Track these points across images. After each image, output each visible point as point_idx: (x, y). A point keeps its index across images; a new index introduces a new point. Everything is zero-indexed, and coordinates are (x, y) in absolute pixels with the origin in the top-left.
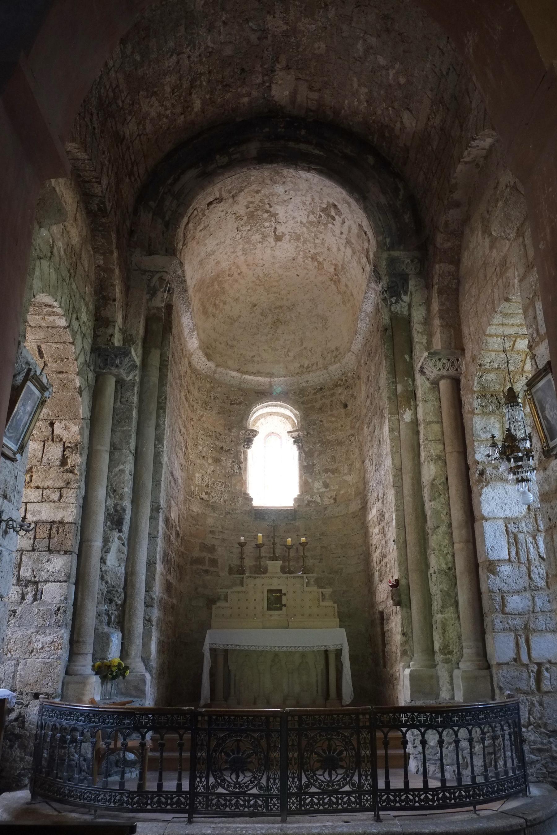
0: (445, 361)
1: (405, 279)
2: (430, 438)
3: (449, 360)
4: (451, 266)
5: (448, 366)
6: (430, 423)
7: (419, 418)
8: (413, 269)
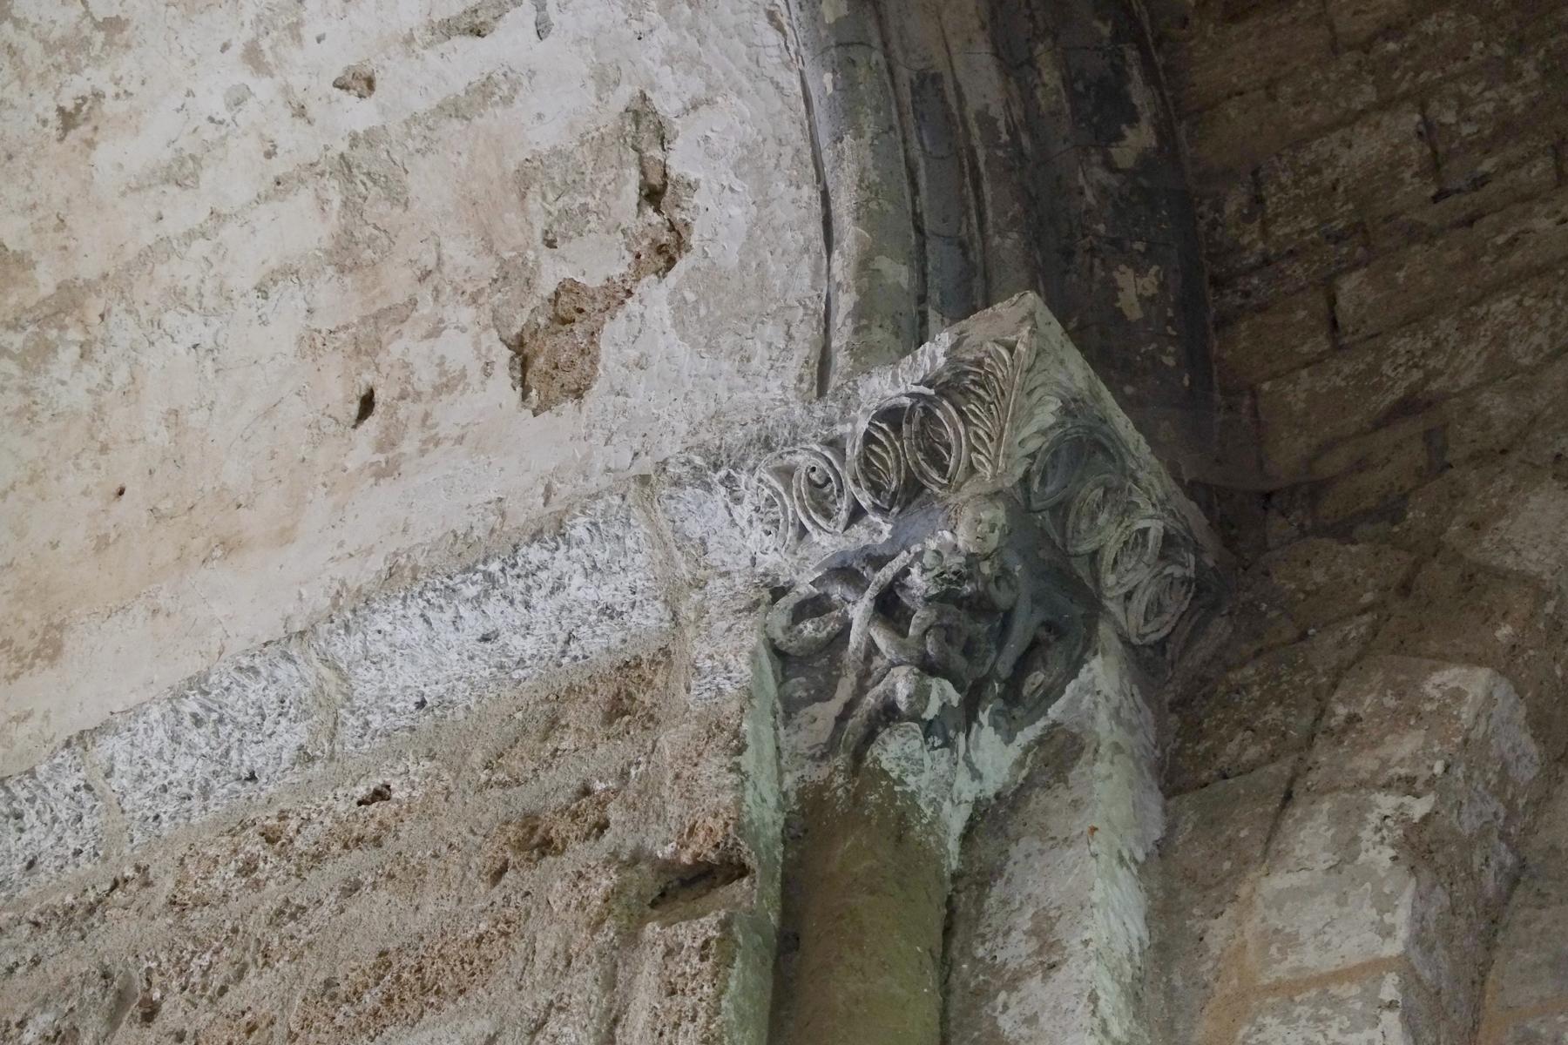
8: (1140, 604)
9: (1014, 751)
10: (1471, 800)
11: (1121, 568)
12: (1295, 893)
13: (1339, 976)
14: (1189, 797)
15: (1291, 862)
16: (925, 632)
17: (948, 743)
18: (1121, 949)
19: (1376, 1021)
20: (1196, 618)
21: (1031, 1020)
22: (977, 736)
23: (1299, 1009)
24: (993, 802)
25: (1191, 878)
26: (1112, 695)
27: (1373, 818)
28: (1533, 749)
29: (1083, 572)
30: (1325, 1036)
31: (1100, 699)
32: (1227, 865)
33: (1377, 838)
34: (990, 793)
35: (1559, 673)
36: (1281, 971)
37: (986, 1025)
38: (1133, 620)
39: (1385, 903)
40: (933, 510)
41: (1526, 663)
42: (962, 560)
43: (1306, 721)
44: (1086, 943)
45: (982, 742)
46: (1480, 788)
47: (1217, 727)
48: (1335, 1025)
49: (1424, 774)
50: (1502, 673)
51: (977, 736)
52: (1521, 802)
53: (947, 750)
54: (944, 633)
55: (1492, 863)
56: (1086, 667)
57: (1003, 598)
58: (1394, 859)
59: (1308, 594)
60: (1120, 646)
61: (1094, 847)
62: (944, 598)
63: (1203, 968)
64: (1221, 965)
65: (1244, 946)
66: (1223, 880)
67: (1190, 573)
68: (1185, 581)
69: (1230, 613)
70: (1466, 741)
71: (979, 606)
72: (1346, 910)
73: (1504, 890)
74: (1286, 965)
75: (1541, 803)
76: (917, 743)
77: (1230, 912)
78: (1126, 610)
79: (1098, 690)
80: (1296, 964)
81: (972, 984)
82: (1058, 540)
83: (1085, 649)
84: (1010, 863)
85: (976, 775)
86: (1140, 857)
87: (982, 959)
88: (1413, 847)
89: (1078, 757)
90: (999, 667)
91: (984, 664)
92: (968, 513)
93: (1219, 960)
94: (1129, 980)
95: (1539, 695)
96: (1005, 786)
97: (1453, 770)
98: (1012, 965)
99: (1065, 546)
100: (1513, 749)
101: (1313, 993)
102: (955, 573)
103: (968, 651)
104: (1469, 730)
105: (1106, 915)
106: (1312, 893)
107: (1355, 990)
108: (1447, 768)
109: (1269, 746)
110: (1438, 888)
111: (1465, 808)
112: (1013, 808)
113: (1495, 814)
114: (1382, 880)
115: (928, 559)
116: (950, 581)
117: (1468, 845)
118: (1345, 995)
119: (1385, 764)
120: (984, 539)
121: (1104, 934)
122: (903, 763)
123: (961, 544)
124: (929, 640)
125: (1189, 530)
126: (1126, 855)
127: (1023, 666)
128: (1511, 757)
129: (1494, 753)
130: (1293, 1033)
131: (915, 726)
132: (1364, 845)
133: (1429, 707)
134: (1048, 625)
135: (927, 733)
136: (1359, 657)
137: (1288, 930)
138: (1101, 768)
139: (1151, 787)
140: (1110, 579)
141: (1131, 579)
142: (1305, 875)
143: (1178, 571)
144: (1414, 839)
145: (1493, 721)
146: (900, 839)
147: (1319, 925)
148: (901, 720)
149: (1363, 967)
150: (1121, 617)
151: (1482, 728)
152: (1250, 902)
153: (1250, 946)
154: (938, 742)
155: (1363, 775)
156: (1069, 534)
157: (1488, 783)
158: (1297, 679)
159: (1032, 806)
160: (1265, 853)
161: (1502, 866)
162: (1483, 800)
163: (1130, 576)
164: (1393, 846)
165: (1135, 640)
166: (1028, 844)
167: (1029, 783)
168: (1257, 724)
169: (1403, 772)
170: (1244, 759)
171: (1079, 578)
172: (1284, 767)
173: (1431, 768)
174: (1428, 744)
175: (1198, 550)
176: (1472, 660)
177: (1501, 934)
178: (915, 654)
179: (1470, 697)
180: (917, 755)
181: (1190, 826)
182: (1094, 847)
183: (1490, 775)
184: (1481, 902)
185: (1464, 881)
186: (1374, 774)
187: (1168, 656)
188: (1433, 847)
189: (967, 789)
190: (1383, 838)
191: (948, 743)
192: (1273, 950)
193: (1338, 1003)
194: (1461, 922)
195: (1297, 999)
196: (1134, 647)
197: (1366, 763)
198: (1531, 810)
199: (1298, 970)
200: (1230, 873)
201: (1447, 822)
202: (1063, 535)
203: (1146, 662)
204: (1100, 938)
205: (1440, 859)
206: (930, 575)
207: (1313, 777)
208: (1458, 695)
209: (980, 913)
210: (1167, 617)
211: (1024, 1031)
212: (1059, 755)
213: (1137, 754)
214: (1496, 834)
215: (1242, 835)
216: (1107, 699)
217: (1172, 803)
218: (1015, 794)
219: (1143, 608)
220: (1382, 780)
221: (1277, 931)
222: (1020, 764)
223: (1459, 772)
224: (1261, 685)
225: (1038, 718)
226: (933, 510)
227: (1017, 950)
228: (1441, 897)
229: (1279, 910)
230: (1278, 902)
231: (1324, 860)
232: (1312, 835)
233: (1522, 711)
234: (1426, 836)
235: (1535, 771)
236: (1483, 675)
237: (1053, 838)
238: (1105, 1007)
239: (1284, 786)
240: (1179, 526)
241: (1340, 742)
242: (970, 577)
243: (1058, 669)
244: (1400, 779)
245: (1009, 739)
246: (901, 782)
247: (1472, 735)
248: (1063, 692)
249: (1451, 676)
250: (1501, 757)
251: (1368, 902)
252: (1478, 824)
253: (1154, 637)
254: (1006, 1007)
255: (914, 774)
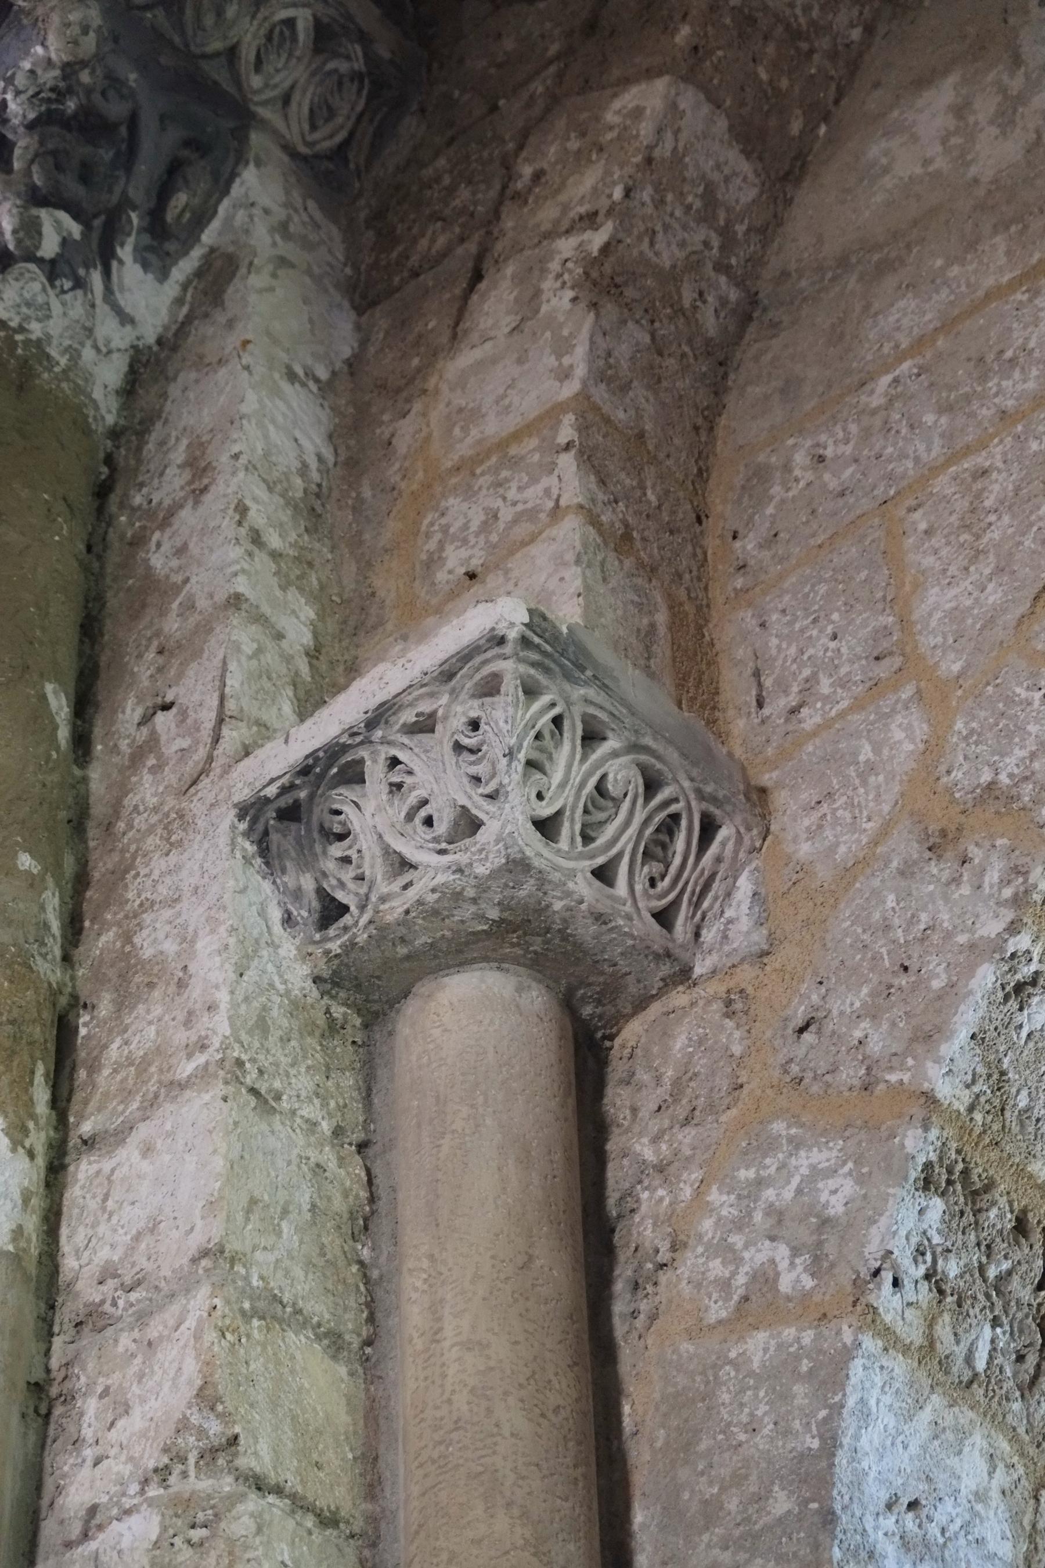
0: (622, 774)
1: (212, 130)
2: (259, 1455)
3: (651, 786)
4: (733, 157)
5: (623, 831)
6: (272, 1310)
7: (69, 1263)
8: (302, 104)
9: (171, 289)
10: (666, 227)
11: (267, 68)
12: (480, 366)
13: (516, 436)
14: (379, 308)
15: (475, 337)
16: (32, 161)
17: (80, 284)
18: (288, 460)
19: (551, 468)
20: (378, 117)
21: (181, 551)
22: (120, 277)
23: (481, 481)
24: (155, 348)
25: (382, 387)
26: (275, 208)
27: (555, 266)
28: (745, 167)
29: (217, 73)
30: (504, 499)
31: (256, 211)
32: (416, 362)
33: (558, 284)
34: (151, 339)
35: (764, 76)
36: (464, 449)
37: (141, 571)
38: (294, 126)
39: (562, 347)
40: (22, 27)
41: (716, 68)
42: (57, 72)
43: (493, 194)
44: (236, 456)
45: (127, 281)
46: (678, 213)
47: (409, 229)
48: (514, 485)
49: (604, 204)
50: (685, 79)
51: (119, 271)
52: (740, 229)
53: (79, 293)
54: (50, 160)
55: (710, 299)
56: (238, 180)
57: (115, 109)
58: (574, 300)
59: (499, 66)
60: (286, 159)
61: (246, 359)
62: (44, 122)
63: (390, 472)
64: (407, 464)
65: (430, 435)
66: (414, 378)
67: (359, 65)
68: (357, 77)
69: (423, 110)
70: (649, 161)
71: (90, 125)
72: (526, 366)
73: (731, 328)
74: (469, 440)
75: (768, 230)
76: (36, 286)
77: (417, 406)
78: (286, 117)
79: (258, 201)
80: (479, 436)
81: (129, 535)
82: (177, 40)
83: (237, 163)
84: (169, 403)
85: (125, 319)
86: (323, 374)
87: (140, 507)
88: (595, 284)
89: (233, 274)
90: (131, 192)
91: (110, 191)
92: (55, 19)
93: (405, 458)
94: (299, 494)
95: (742, 104)
96: (166, 328)
97: (636, 195)
98: (167, 502)
99: (187, 45)
100: (718, 167)
101: (494, 459)
102: (52, 90)
103: (86, 175)
104: (651, 148)
105: (260, 425)
106: (494, 361)
107: (534, 442)
108: (628, 193)
109: (457, 230)
110: (631, 325)
111: (660, 236)
112: (175, 349)
113: (706, 244)
114: (561, 326)
115: (20, 81)
116: (49, 100)
117: (672, 277)
118: (523, 452)
119: (565, 208)
120: (76, 43)
121: (259, 446)
122: (24, 310)
123: (53, 56)
124: (35, 168)
125: (350, 17)
126: (299, 370)
127: (163, 193)
128: (716, 176)
129: (691, 173)
130: (474, 506)
131: (32, 267)
132: (544, 297)
133: (609, 136)
134: (187, 143)
135: (52, 277)
136: (548, 110)
137: (471, 405)
138: (256, 281)
139: (339, 306)
140: (256, 81)
141: (283, 80)
142: (488, 345)
143: (344, 67)
144: (595, 274)
145: (684, 136)
146: (21, 388)
147: (501, 391)
148: (16, 262)
149: (540, 418)
150: (278, 123)
151: (668, 144)
152: (437, 391)
153: (435, 434)
154: (68, 284)
155: (546, 226)
156: (190, 32)
157: (689, 207)
158: (485, 154)
159: (191, 339)
160: (454, 337)
161: (723, 301)
162: (685, 227)
163: (282, 75)
164: (573, 288)
165: (303, 149)
166: (188, 376)
167: (189, 319)
168: (447, 212)
169: (582, 210)
170: (433, 251)
171: (215, 83)
172: (472, 247)
173: (610, 196)
174: (608, 173)
175: (364, 38)
176: (650, 74)
177: (732, 376)
178: (23, 188)
179: (648, 112)
180: (40, 299)
181: (381, 335)
182: (246, 359)
183: (690, 199)
184: (698, 342)
185: (671, 319)
186: (557, 222)
187: (352, 166)
188: (618, 280)
189: (120, 337)
190: (564, 283)
191: (80, 284)
192: (457, 431)
193: (515, 463)
194: (671, 363)
195: (478, 471)
196: (305, 159)
197: (547, 214)
198: (755, 238)
199: (479, 442)
200: (419, 370)
201: (635, 252)
202: (183, 33)
203: (326, 175)
204: (253, 450)
205: (630, 293)
206: (23, 97)
207: (499, 246)
208: (638, 113)
209: (139, 461)
210: (340, 120)
211: (175, 563)
212: (217, 278)
213: (316, 270)
214: (710, 265)
215: (430, 327)
216: (267, 211)
217: (364, 318)
218: (176, 335)
219: (306, 110)
220: (565, 224)
221: (460, 410)
222: (179, 301)
223: (646, 195)
224: (451, 172)
225: (192, 247)
226: (22, 27)
227: (172, 483)
228: (638, 334)
229: (463, 389)
230: (461, 384)
231: (508, 321)
232: (495, 306)
233: (722, 124)
234: (607, 268)
235: (752, 193)
236: (661, 84)
237: (209, 365)
238: (256, 516)
239: (470, 265)
240: (332, 12)
241: (526, 202)
242: (70, 91)
243: (203, 186)
244: (581, 218)
245: (163, 275)
246: (21, 329)
247: (657, 153)
248: (215, 212)
249: (629, 98)
250: (703, 177)
251: (548, 350)
252: (680, 254)
253: (327, 144)
254: (159, 545)
255: (39, 320)
